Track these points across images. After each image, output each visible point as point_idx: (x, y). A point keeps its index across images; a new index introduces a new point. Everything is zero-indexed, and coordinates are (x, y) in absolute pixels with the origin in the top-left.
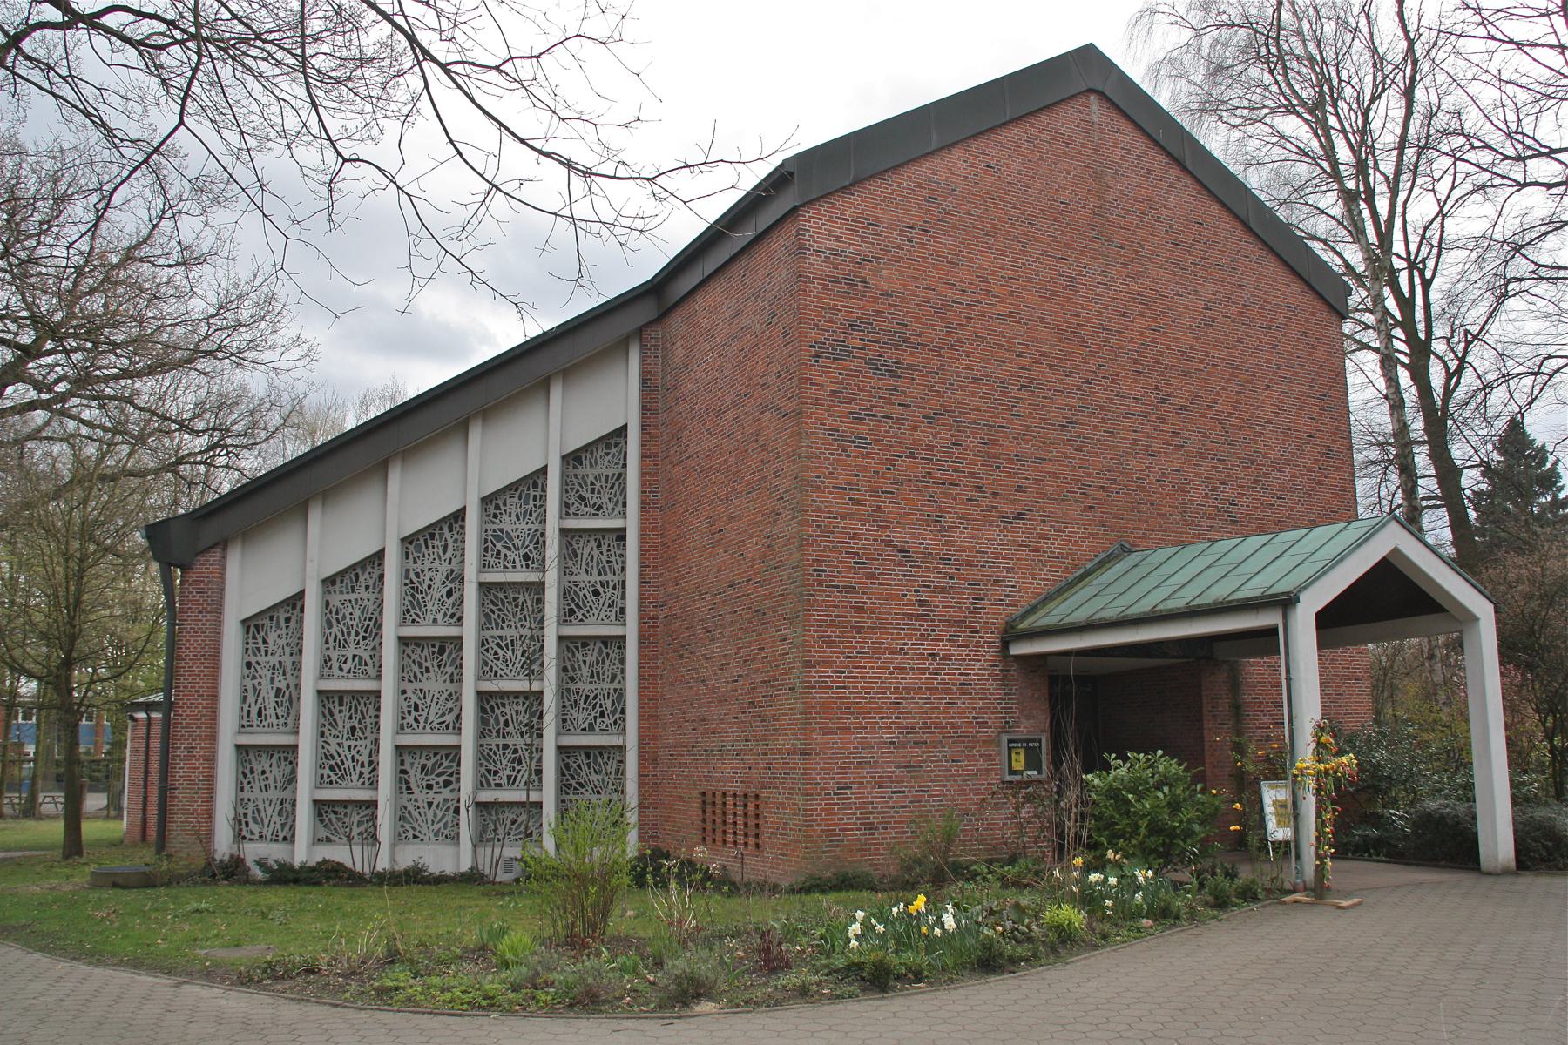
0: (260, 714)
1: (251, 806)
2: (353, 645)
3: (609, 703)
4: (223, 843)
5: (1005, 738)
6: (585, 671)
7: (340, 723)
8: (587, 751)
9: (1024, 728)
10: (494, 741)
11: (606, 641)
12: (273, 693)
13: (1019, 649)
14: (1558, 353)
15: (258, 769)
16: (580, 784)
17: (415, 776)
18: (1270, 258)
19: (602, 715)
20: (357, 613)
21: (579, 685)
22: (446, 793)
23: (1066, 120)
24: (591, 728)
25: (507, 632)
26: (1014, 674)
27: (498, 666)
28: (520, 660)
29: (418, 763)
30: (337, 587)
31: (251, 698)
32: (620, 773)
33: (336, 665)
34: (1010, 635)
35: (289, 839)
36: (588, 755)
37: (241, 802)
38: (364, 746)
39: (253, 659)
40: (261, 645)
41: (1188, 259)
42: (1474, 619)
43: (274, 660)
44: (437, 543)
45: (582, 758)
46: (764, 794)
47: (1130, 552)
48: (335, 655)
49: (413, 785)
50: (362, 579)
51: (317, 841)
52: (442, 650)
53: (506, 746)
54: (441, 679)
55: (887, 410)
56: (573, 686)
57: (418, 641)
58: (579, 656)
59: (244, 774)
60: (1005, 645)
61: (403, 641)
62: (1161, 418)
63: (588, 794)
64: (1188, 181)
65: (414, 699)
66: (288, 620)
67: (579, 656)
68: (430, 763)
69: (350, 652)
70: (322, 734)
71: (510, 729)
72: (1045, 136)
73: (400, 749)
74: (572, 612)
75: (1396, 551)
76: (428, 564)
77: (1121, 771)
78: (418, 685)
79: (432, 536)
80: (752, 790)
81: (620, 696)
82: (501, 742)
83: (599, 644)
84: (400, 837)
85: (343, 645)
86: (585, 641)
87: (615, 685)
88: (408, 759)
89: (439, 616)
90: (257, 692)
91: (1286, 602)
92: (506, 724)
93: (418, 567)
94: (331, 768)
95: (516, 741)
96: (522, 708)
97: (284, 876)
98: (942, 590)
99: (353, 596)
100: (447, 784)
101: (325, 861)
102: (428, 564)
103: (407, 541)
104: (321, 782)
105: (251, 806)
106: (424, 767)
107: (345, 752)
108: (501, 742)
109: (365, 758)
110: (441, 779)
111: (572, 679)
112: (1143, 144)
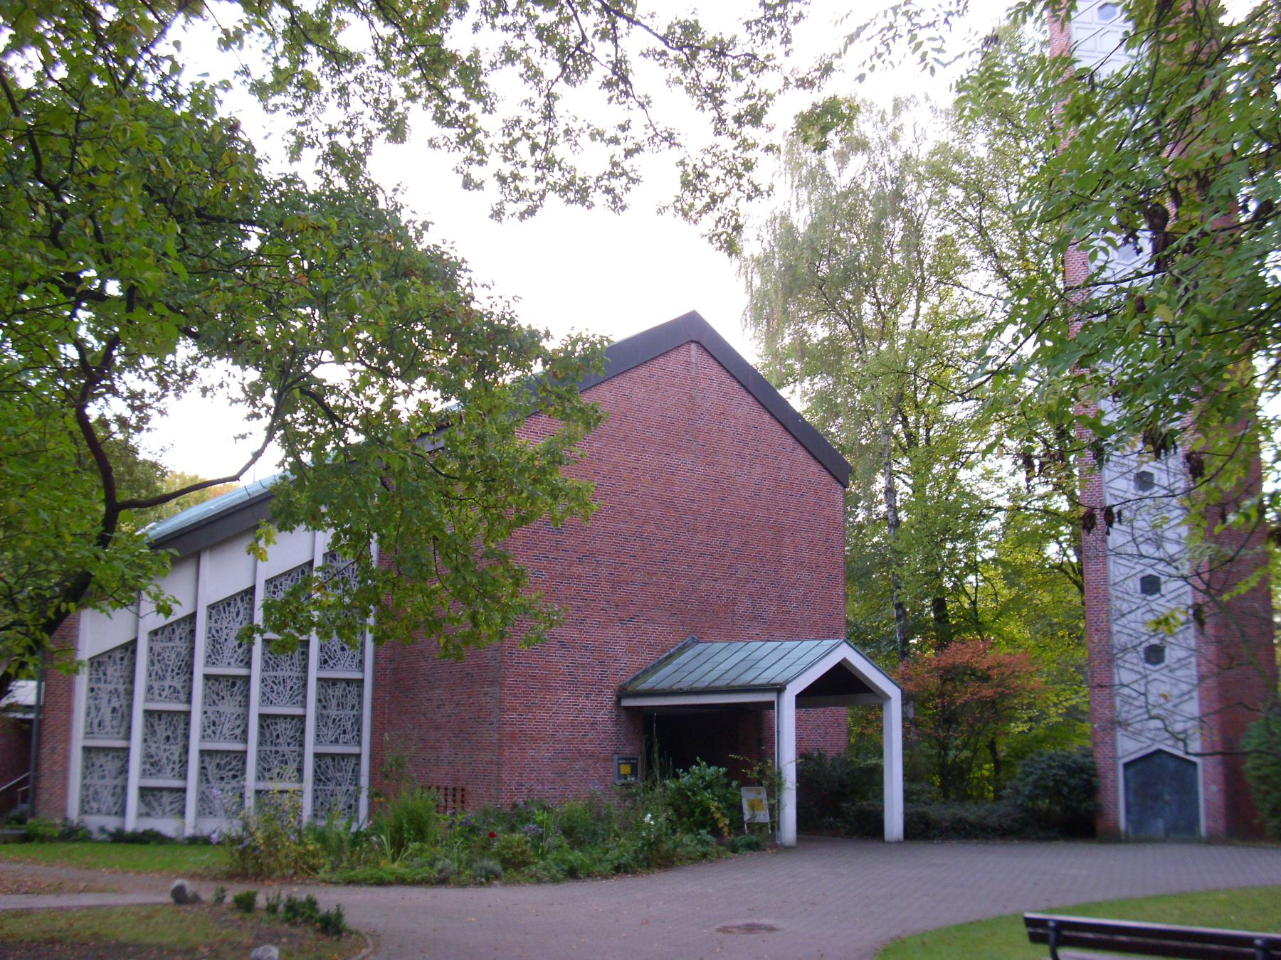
0: (100, 725)
1: (92, 790)
2: (169, 678)
3: (349, 724)
4: (73, 811)
5: (616, 757)
6: (334, 702)
7: (159, 733)
8: (333, 756)
9: (628, 750)
10: (268, 748)
11: (348, 682)
12: (109, 710)
13: (627, 703)
14: (795, 669)
15: (98, 763)
16: (328, 780)
17: (212, 772)
18: (800, 449)
19: (344, 732)
20: (173, 656)
21: (329, 711)
22: (234, 783)
23: (674, 362)
24: (337, 741)
25: (279, 674)
26: (623, 717)
27: (273, 696)
28: (289, 693)
29: (214, 763)
30: (159, 637)
31: (93, 713)
32: (356, 773)
33: (157, 692)
34: (622, 693)
35: (122, 812)
36: (333, 760)
37: (85, 787)
38: (176, 750)
39: (95, 686)
40: (101, 675)
41: (746, 452)
42: (887, 698)
43: (111, 687)
44: (232, 609)
45: (329, 761)
46: (469, 788)
47: (698, 642)
48: (156, 685)
49: (210, 777)
50: (177, 632)
51: (140, 815)
52: (234, 685)
53: (277, 752)
54: (232, 704)
55: (555, 554)
56: (325, 712)
57: (216, 678)
58: (330, 691)
59: (88, 767)
60: (619, 700)
61: (207, 677)
62: (723, 556)
63: (331, 786)
64: (750, 399)
65: (213, 718)
66: (122, 659)
67: (330, 691)
68: (223, 763)
69: (167, 683)
70: (145, 740)
71: (280, 740)
72: (661, 373)
73: (203, 753)
74: (326, 662)
75: (845, 660)
76: (225, 624)
77: (685, 779)
78: (216, 708)
79: (229, 605)
80: (460, 785)
81: (358, 720)
82: (274, 749)
83: (344, 684)
84: (200, 813)
85: (163, 678)
86: (334, 682)
87: (354, 712)
88: (207, 759)
89: (232, 661)
90: (98, 709)
91: (779, 689)
92: (278, 736)
93: (218, 626)
94: (152, 764)
95: (283, 748)
96: (289, 726)
97: (120, 837)
98: (583, 665)
99: (170, 644)
100: (234, 777)
101: (151, 830)
102: (225, 624)
103: (212, 607)
104: (144, 773)
105: (92, 790)
106: (218, 765)
107: (161, 753)
108: (274, 749)
109: (176, 757)
110: (231, 773)
111: (325, 707)
112: (723, 375)
